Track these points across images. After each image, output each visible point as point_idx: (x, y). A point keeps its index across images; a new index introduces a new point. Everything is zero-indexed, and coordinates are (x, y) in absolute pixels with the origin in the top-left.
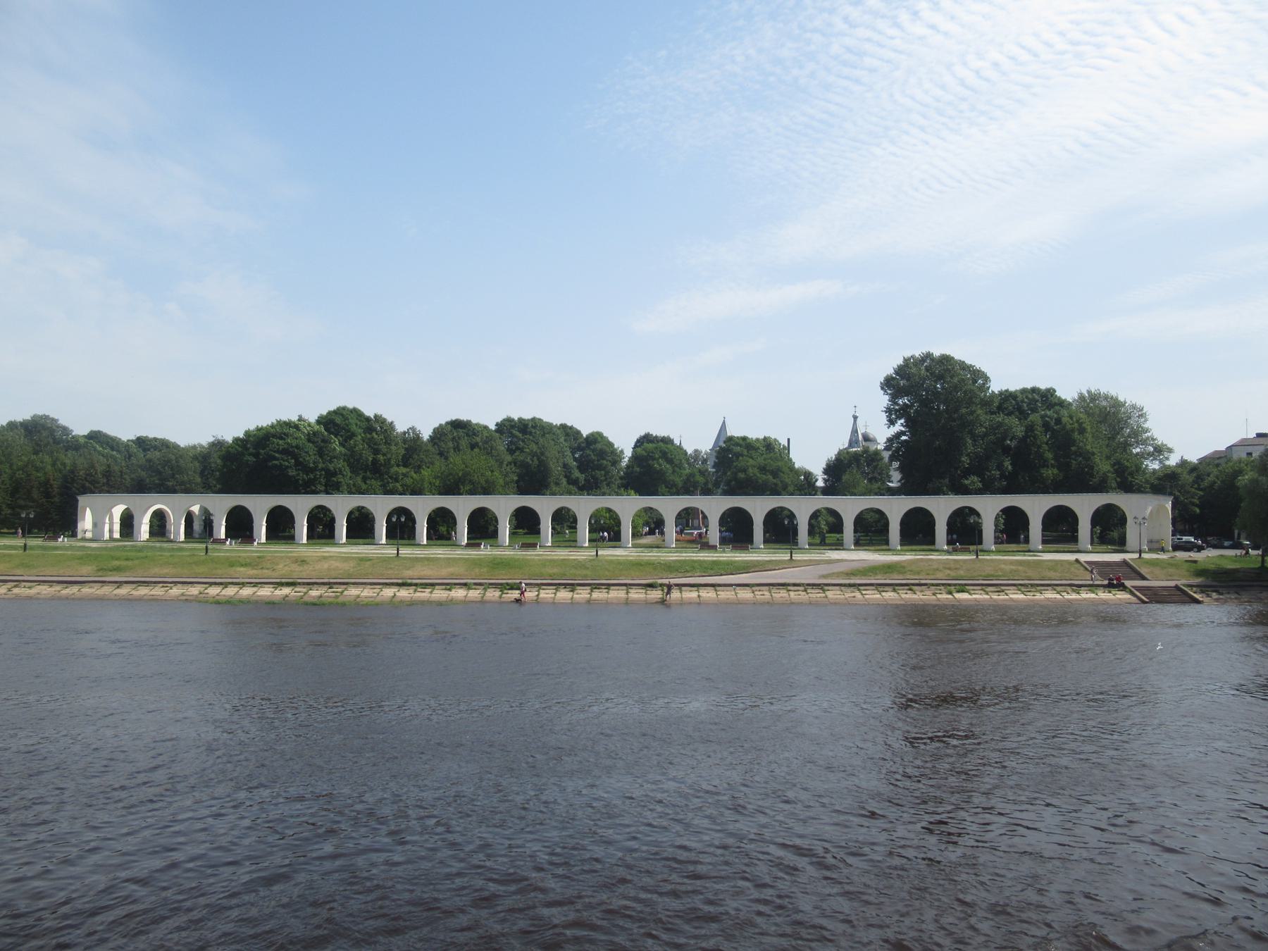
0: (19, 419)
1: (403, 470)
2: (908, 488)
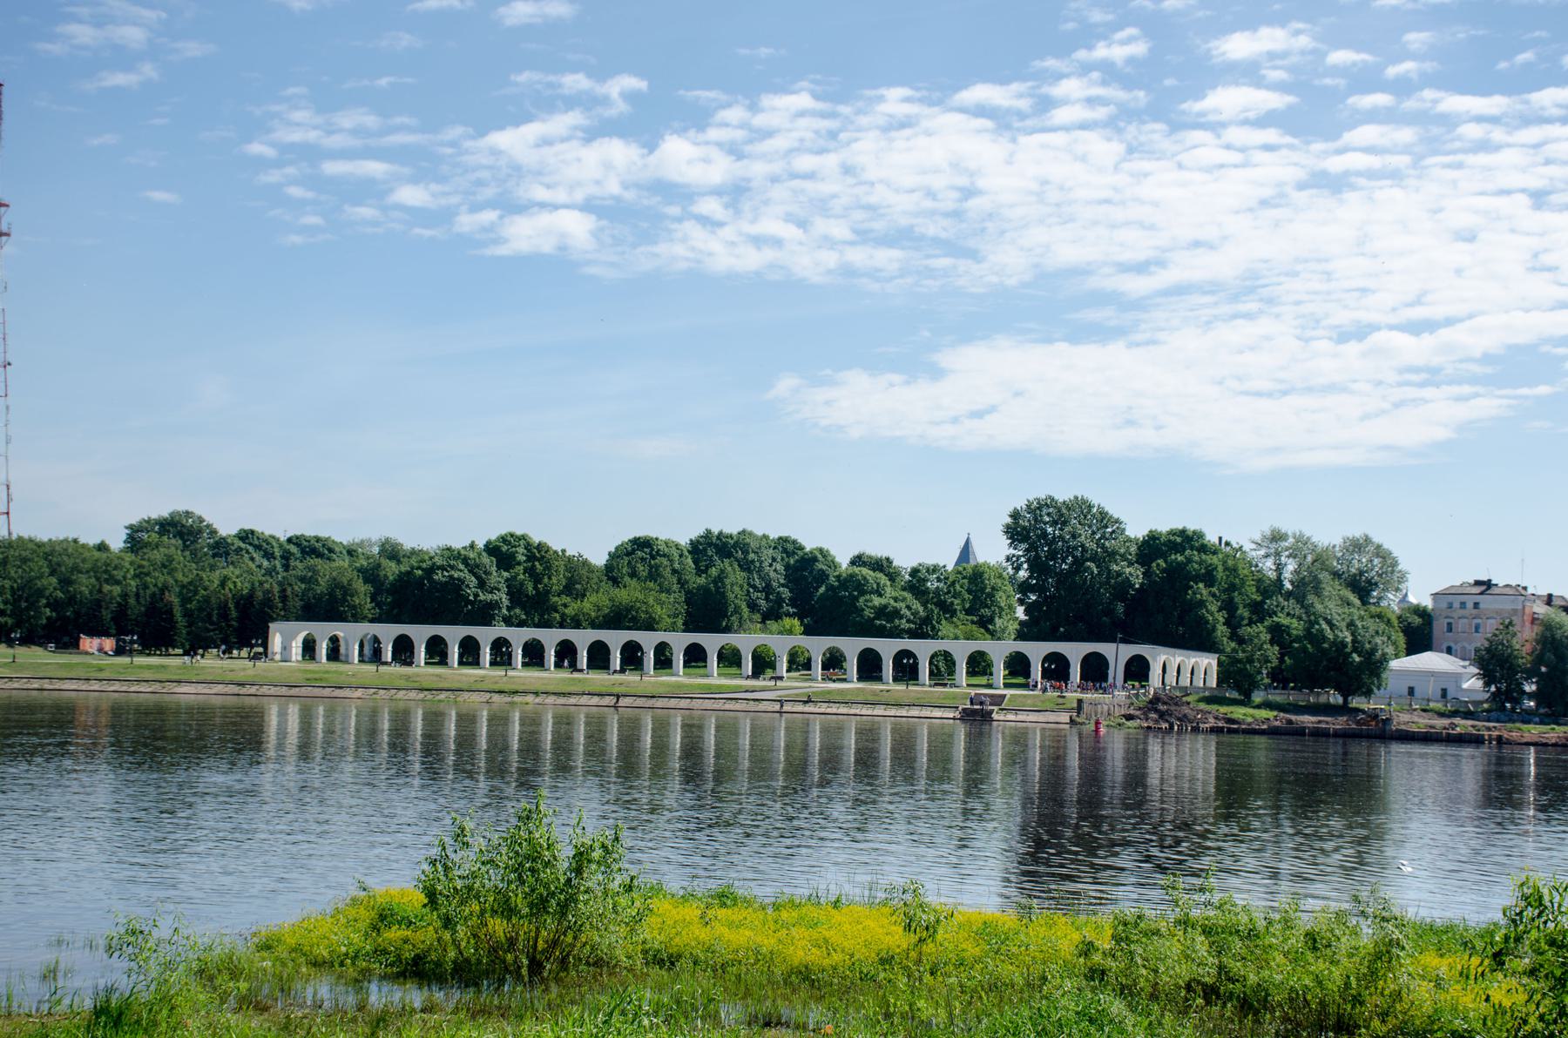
0: (154, 516)
1: (565, 599)
2: (689, 627)
